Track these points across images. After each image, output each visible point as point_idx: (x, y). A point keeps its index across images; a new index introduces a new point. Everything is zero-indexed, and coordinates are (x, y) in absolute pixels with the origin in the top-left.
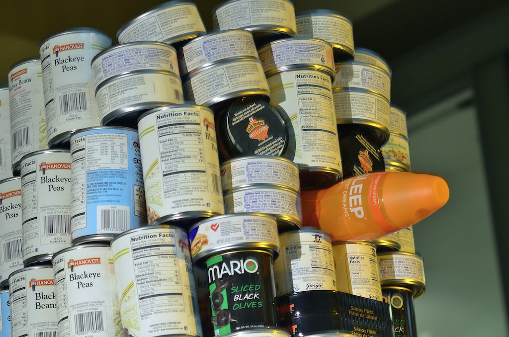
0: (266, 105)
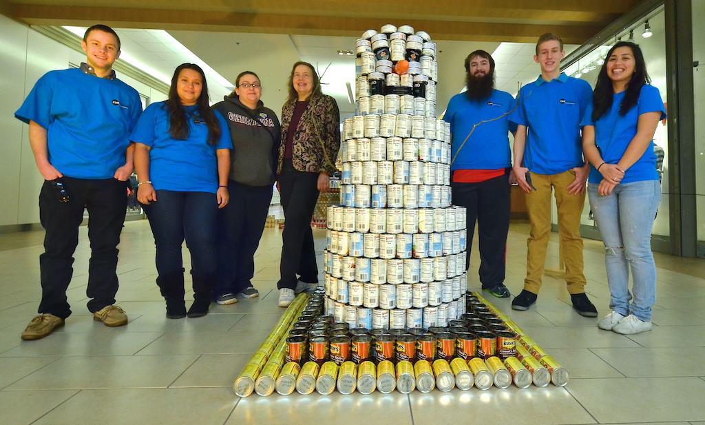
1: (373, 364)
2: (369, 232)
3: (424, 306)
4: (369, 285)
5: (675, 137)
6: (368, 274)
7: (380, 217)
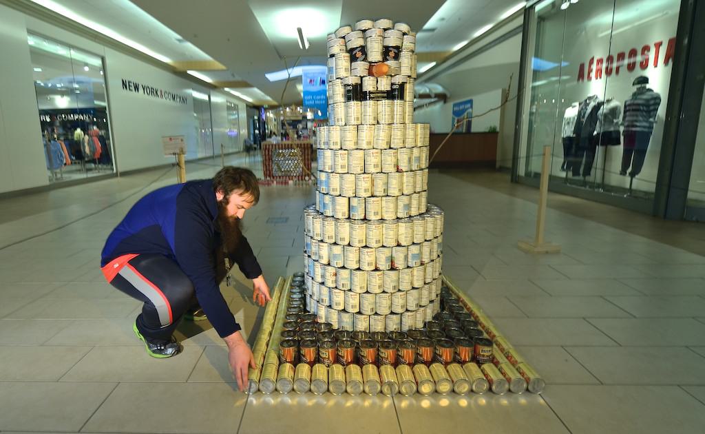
0: (363, 49)
1: (358, 368)
2: (349, 245)
3: (366, 196)
4: (350, 293)
5: (679, 85)
6: (349, 283)
7: (359, 232)
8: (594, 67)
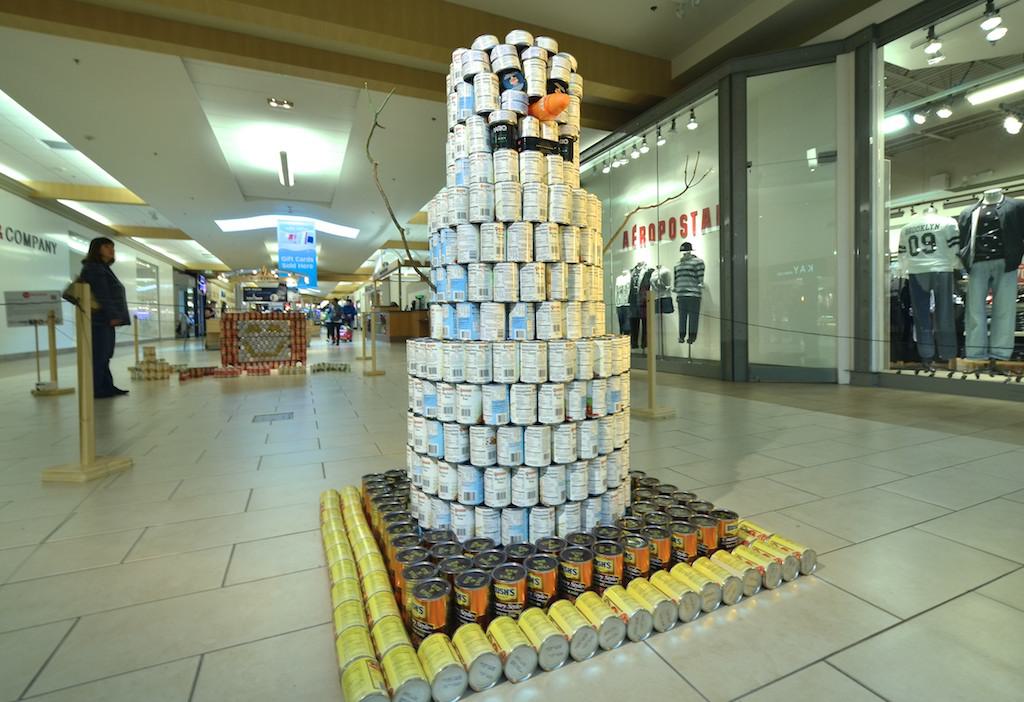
0: (518, 73)
8: (637, 234)
